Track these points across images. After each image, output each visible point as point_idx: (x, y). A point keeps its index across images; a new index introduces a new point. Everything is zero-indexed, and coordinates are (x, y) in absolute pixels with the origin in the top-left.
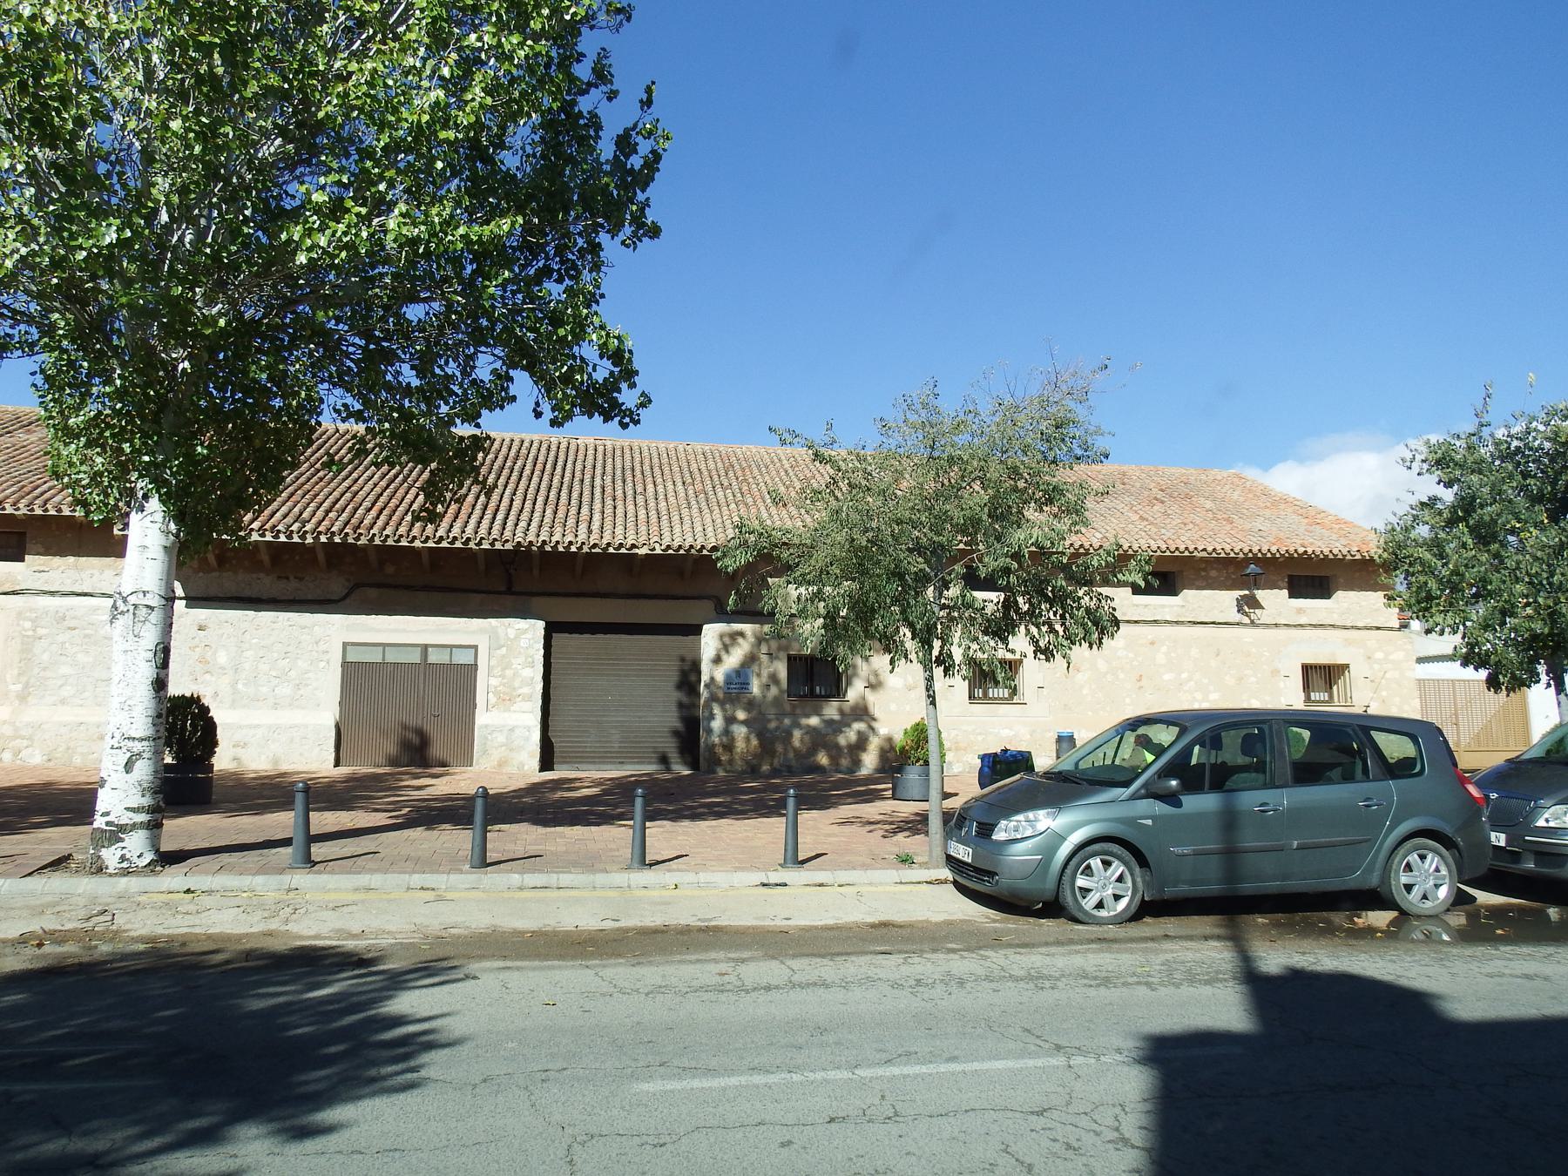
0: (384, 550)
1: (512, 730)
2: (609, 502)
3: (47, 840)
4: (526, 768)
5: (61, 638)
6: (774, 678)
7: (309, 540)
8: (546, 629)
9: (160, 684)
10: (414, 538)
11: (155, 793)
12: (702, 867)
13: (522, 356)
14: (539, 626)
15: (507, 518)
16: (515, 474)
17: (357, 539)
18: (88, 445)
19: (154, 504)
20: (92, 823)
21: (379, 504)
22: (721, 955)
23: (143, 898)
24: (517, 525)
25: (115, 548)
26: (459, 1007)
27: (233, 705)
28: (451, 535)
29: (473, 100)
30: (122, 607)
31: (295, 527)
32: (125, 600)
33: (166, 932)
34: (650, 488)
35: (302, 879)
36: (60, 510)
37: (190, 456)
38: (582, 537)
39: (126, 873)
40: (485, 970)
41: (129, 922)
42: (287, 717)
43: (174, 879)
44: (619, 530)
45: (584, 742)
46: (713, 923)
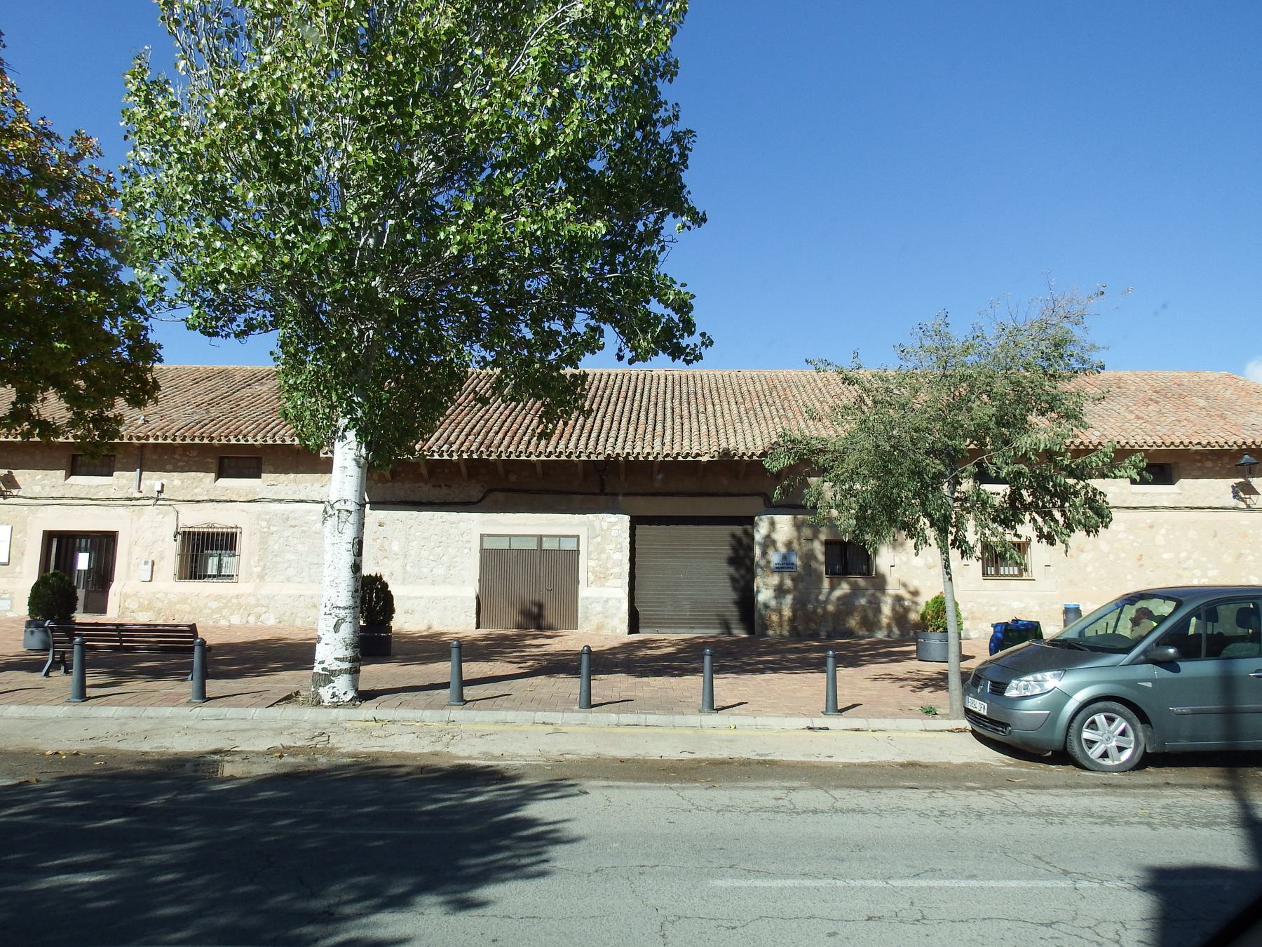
0: (508, 462)
2: (677, 420)
3: (279, 682)
4: (618, 631)
5: (286, 534)
7: (455, 457)
8: (630, 522)
9: (356, 568)
11: (355, 647)
12: (757, 713)
13: (607, 314)
15: (599, 436)
16: (605, 401)
17: (489, 455)
20: (312, 668)
21: (505, 428)
22: (776, 783)
23: (348, 725)
24: (607, 441)
25: (325, 467)
27: (404, 583)
28: (558, 450)
30: (330, 512)
31: (444, 448)
32: (332, 507)
33: (365, 750)
34: (710, 407)
35: (457, 713)
36: (284, 441)
38: (657, 448)
39: (336, 705)
41: (340, 742)
43: (367, 711)
44: (686, 442)
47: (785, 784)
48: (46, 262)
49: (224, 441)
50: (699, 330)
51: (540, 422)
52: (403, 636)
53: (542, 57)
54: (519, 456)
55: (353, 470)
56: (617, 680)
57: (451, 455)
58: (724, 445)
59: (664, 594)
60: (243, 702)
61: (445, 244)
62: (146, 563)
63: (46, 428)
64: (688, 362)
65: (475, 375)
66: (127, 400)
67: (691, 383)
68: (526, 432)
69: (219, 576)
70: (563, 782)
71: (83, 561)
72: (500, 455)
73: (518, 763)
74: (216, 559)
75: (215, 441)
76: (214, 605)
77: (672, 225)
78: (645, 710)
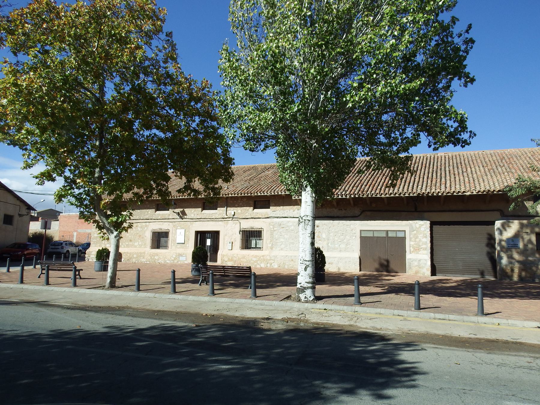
0: (372, 198)
1: (420, 260)
2: (452, 176)
4: (426, 274)
5: (280, 231)
6: (530, 241)
7: (348, 197)
8: (430, 224)
9: (313, 244)
10: (382, 194)
11: (313, 278)
12: (508, 317)
14: (428, 223)
15: (414, 185)
17: (363, 195)
18: (290, 172)
19: (309, 189)
20: (296, 285)
21: (369, 183)
22: (526, 354)
23: (313, 310)
24: (417, 187)
25: (298, 203)
26: (422, 360)
27: (328, 251)
28: (394, 192)
29: (405, 40)
30: (301, 221)
31: (343, 193)
32: (302, 219)
33: (321, 322)
34: (469, 169)
35: (358, 308)
36: (278, 193)
37: (319, 174)
38: (443, 189)
39: (307, 302)
40: (429, 347)
41: (310, 317)
42: (344, 255)
43: (320, 305)
44: (458, 186)
45: (449, 266)
46: (518, 341)
47: (532, 355)
48: (194, 128)
49: (256, 194)
50: (469, 130)
51: (390, 179)
52: (330, 274)
54: (377, 195)
55: (310, 203)
57: (346, 196)
60: (271, 299)
61: (347, 102)
62: (230, 243)
66: (223, 180)
67: (458, 158)
68: (379, 185)
69: (256, 248)
71: (209, 242)
73: (390, 333)
74: (254, 241)
75: (253, 195)
76: (255, 259)
78: (448, 312)
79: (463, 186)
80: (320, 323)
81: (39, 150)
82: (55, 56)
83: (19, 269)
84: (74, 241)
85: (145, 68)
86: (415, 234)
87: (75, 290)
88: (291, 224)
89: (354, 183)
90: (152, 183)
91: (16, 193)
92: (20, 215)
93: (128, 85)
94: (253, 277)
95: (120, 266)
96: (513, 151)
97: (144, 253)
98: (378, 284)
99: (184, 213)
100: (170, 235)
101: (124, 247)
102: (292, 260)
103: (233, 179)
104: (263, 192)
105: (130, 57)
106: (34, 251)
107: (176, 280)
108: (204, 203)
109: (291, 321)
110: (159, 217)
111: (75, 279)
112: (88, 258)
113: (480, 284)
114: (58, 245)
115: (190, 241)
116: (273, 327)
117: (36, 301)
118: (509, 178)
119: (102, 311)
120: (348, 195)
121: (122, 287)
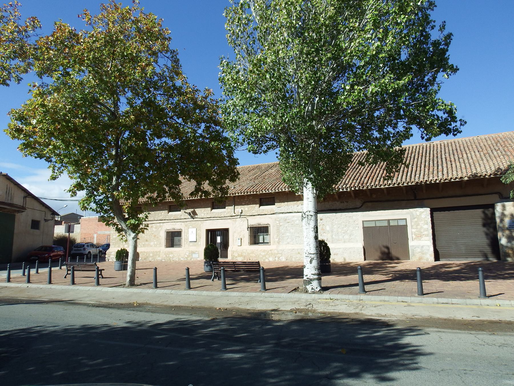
0: (372, 190)
2: (449, 163)
3: (291, 283)
4: (429, 260)
5: (286, 225)
7: (349, 190)
9: (316, 238)
11: (318, 269)
13: (414, 120)
15: (411, 174)
16: (412, 159)
17: (363, 188)
19: (310, 185)
20: (303, 278)
21: (368, 176)
23: (319, 301)
24: (415, 176)
25: (300, 198)
26: (425, 343)
27: (332, 242)
28: (393, 183)
30: (304, 216)
31: (344, 186)
32: (305, 214)
33: (328, 311)
34: (465, 155)
35: (363, 297)
36: (282, 190)
40: (432, 331)
41: (317, 307)
43: (326, 295)
44: (455, 173)
45: (451, 250)
48: (201, 134)
49: (261, 192)
50: (458, 119)
53: (373, 17)
54: (376, 187)
56: (433, 282)
58: (474, 171)
59: (451, 243)
62: (239, 239)
63: (207, 193)
64: (454, 135)
65: (356, 155)
66: (229, 180)
68: (378, 176)
69: (264, 243)
70: (415, 328)
71: (219, 239)
72: (368, 187)
73: (394, 319)
75: (258, 193)
76: (263, 254)
77: (442, 76)
79: (460, 172)
80: (327, 312)
81: (62, 161)
82: (75, 77)
83: (47, 270)
84: (95, 242)
85: (155, 83)
86: (416, 221)
87: (99, 288)
88: (296, 219)
89: (353, 176)
90: (165, 187)
91: (42, 200)
92: (46, 220)
93: (139, 99)
94: (261, 271)
95: (138, 265)
96: (508, 134)
97: (160, 252)
98: (383, 273)
99: (194, 213)
100: (183, 234)
101: (141, 247)
102: (299, 253)
103: (239, 179)
104: (268, 190)
105: (142, 74)
106: (59, 253)
107: (190, 277)
108: (213, 203)
109: (299, 312)
110: (172, 218)
111: (98, 278)
112: (109, 258)
113: (480, 267)
114: (81, 247)
115: (201, 239)
116: (283, 318)
117: (63, 300)
118: (505, 161)
119: (124, 308)
120: (348, 189)
121: (141, 285)
